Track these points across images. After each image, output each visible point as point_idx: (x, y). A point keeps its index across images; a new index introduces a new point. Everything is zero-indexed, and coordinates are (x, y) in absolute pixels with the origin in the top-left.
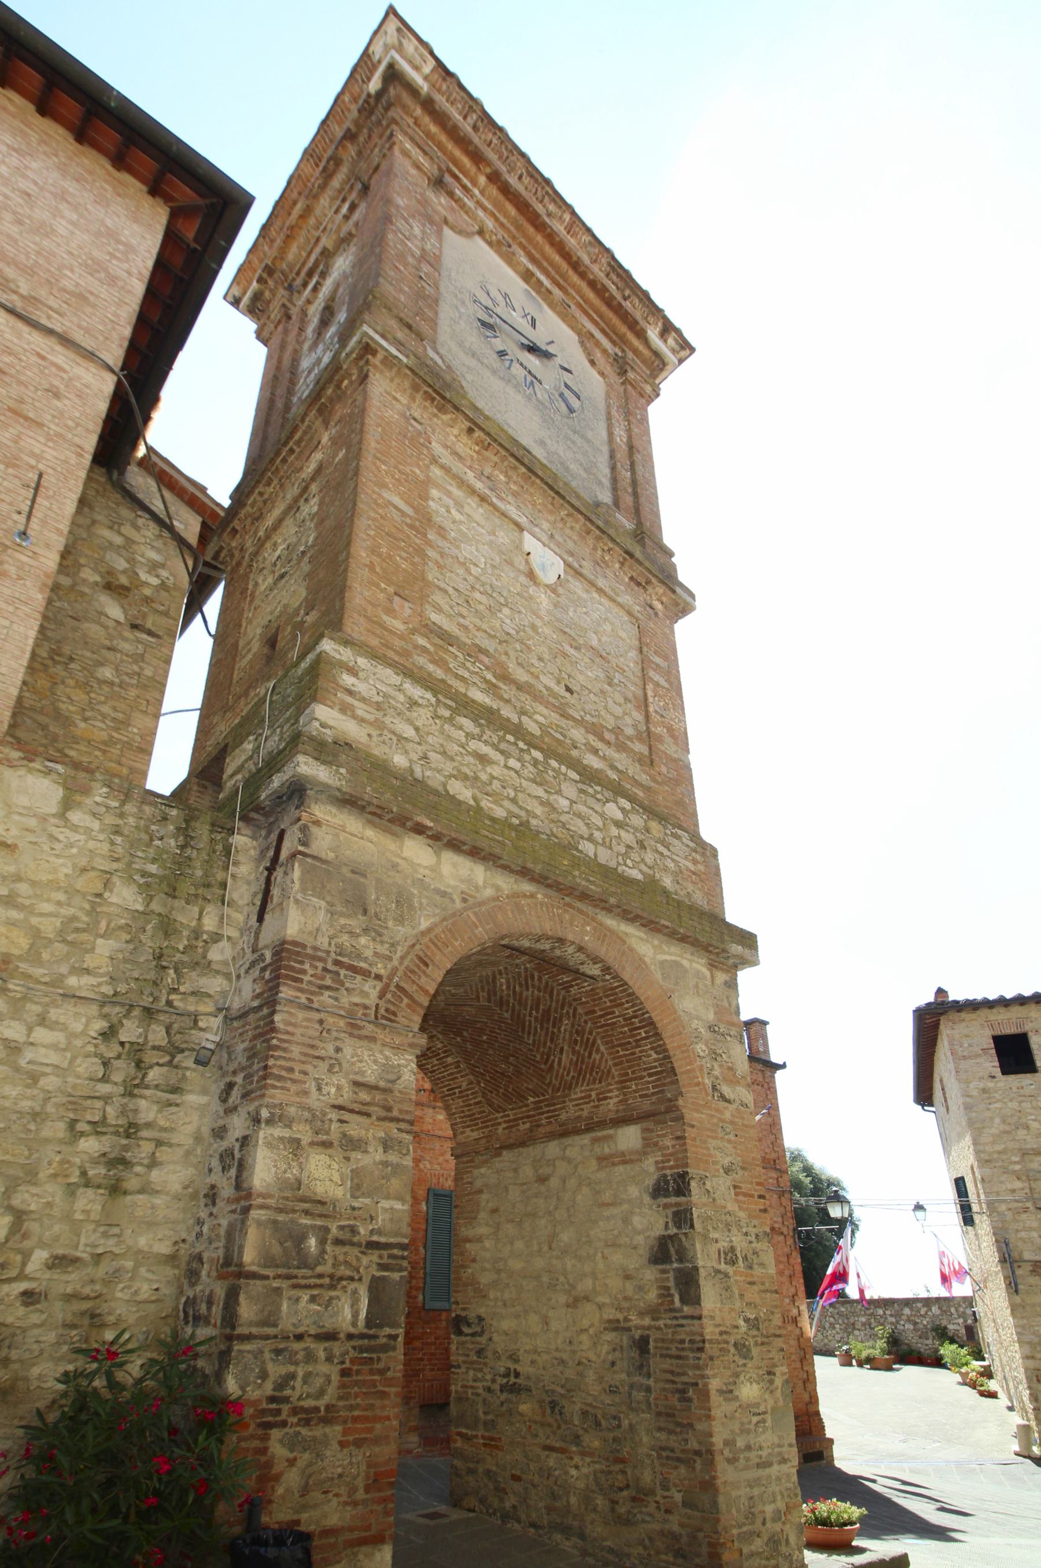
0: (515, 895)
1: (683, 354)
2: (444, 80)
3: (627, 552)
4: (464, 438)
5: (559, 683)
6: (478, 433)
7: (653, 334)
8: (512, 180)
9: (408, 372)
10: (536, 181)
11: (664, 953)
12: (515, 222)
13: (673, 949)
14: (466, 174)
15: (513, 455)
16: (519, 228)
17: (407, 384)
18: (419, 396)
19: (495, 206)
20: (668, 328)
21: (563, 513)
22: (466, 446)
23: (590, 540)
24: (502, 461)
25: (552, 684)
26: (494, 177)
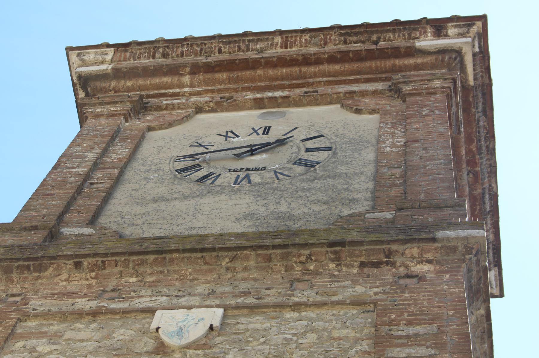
2: (126, 51)
3: (332, 244)
6: (86, 263)
8: (215, 57)
10: (235, 42)
12: (230, 80)
15: (132, 254)
16: (237, 80)
18: (15, 276)
19: (207, 85)
20: (439, 26)
22: (79, 281)
23: (278, 265)
24: (127, 266)
26: (195, 69)
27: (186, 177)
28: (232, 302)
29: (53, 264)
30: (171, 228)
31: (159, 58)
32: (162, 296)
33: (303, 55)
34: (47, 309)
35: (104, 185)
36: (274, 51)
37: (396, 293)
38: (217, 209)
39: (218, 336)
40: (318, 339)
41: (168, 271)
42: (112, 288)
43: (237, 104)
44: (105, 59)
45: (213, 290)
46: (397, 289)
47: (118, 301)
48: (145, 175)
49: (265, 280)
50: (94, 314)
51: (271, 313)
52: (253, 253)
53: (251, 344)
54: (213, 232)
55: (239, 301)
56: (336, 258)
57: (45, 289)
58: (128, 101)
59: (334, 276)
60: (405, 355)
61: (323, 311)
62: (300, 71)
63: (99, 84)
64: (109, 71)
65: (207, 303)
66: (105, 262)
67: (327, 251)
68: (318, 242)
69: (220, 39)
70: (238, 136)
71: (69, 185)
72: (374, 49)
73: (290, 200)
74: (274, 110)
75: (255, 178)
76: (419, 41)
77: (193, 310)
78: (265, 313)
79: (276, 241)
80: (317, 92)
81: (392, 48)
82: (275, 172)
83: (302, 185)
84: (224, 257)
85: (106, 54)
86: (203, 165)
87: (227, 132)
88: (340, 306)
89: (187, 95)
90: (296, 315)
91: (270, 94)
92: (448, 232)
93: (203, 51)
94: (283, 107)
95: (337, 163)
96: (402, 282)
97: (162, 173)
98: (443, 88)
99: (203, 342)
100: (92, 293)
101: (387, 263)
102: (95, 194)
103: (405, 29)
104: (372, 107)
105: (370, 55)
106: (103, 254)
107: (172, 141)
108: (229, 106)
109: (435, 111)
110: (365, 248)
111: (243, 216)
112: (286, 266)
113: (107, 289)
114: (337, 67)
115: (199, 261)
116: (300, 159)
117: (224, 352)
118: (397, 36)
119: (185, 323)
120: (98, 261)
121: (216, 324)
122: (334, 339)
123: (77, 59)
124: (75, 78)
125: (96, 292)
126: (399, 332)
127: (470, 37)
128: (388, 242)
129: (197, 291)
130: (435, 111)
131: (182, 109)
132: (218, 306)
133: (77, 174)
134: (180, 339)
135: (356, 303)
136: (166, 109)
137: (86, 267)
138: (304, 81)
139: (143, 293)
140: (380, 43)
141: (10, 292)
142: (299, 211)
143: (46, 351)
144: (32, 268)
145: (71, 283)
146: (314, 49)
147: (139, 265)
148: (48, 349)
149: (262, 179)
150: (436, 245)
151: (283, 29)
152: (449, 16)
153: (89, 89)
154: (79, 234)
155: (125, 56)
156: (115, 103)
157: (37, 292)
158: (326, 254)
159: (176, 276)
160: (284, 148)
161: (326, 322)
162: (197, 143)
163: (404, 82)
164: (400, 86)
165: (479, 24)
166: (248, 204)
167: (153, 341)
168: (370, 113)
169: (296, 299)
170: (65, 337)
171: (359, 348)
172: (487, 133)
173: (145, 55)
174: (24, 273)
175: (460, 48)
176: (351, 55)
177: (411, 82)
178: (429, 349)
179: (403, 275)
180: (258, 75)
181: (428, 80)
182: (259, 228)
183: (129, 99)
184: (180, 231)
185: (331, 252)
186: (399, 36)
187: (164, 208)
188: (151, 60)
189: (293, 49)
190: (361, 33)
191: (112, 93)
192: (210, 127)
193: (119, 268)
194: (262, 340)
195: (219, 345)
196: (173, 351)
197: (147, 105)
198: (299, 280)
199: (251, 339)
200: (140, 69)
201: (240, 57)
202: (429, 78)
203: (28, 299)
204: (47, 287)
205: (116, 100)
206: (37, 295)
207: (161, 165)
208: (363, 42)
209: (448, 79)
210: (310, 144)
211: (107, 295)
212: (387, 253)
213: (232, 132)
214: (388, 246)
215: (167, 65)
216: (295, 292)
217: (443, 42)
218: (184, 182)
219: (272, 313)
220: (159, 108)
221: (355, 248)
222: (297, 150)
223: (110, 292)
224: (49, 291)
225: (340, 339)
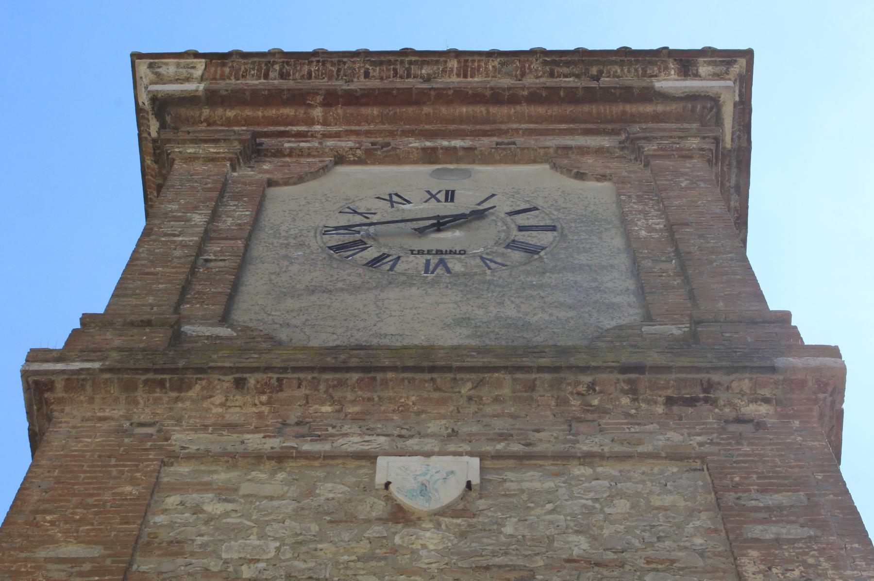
2: (224, 65)
3: (625, 369)
6: (252, 380)
8: (359, 84)
9: (107, 376)
10: (389, 62)
14: (294, 122)
15: (324, 369)
16: (393, 120)
17: (115, 391)
18: (141, 395)
19: (348, 123)
20: (686, 61)
21: (466, 389)
22: (242, 407)
26: (331, 99)
28: (489, 448)
29: (201, 379)
30: (349, 333)
31: (275, 79)
32: (378, 435)
33: (492, 89)
34: (202, 447)
35: (227, 264)
36: (448, 80)
38: (411, 309)
39: (481, 498)
40: (632, 507)
41: (380, 398)
42: (296, 420)
43: (396, 155)
44: (191, 74)
45: (453, 430)
46: (729, 438)
47: (311, 440)
48: (283, 252)
49: (528, 418)
50: (280, 458)
51: (548, 464)
53: (533, 512)
54: (417, 342)
55: (500, 446)
56: (631, 389)
57: (190, 417)
58: (236, 140)
59: (632, 416)
60: (772, 536)
61: (627, 466)
62: (488, 112)
63: (184, 112)
64: (201, 94)
65: (451, 447)
66: (282, 380)
67: (618, 379)
68: (605, 365)
70: (409, 202)
71: (175, 260)
72: (595, 88)
74: (451, 167)
75: (455, 265)
76: (659, 81)
78: (540, 466)
80: (514, 143)
81: (621, 88)
82: (482, 258)
83: (528, 279)
85: (193, 68)
86: (370, 242)
87: (390, 195)
88: (652, 461)
89: (319, 136)
90: (588, 471)
91: (445, 143)
92: (791, 359)
93: (342, 72)
94: (464, 163)
95: (571, 250)
96: (732, 428)
97: (308, 251)
98: (702, 149)
99: (461, 506)
100: (267, 426)
101: (706, 400)
102: (218, 277)
103: (637, 61)
104: (600, 170)
105: (590, 96)
107: (309, 203)
108: (386, 156)
109: (699, 183)
110: (673, 376)
111: (454, 320)
112: (557, 399)
113: (288, 422)
114: (541, 110)
115: (427, 385)
116: (514, 241)
118: (626, 71)
119: (428, 477)
120: (271, 378)
121: (476, 481)
122: (657, 508)
123: (148, 71)
124: (144, 98)
126: (753, 502)
127: (730, 79)
128: (708, 370)
129: (429, 431)
130: (699, 183)
131: (314, 156)
132: (471, 454)
133: (183, 245)
135: (675, 456)
136: (290, 155)
137: (252, 387)
138: (493, 127)
139: (346, 429)
140: (602, 79)
141: (135, 419)
142: (536, 318)
143: (219, 512)
144: (168, 385)
146: (505, 82)
147: (334, 387)
148: (222, 509)
149: (465, 266)
150: (776, 377)
152: (700, 48)
153: (168, 119)
154: (211, 336)
156: (216, 141)
157: (179, 420)
158: (616, 383)
159: (392, 407)
160: (483, 223)
161: (637, 483)
162: (349, 208)
163: (645, 138)
164: (641, 143)
165: (742, 62)
166: (455, 303)
167: (383, 503)
168: (598, 180)
169: (585, 448)
170: (241, 493)
171: (698, 523)
172: (738, 218)
173: (252, 72)
174: (155, 392)
175: (717, 94)
176: (562, 93)
177: (656, 138)
178: (806, 529)
179: (731, 419)
180: (426, 114)
181: (680, 138)
182: (484, 339)
184: (364, 339)
185: (624, 381)
186: (629, 71)
187: (328, 302)
188: (263, 81)
190: (575, 63)
192: (360, 185)
193: (303, 391)
194: (549, 507)
195: (485, 512)
197: (260, 148)
198: (579, 420)
199: (532, 505)
200: (248, 93)
201: (399, 86)
202: (681, 134)
204: (194, 414)
205: (216, 137)
206: (181, 426)
207: (302, 238)
208: (577, 76)
209: (708, 137)
210: (521, 220)
212: (705, 385)
214: (707, 376)
215: (288, 90)
216: (580, 438)
218: (348, 266)
219: (552, 467)
220: (279, 153)
221: (660, 376)
222: (505, 228)
223: (294, 425)
224: (198, 421)
225: (665, 509)
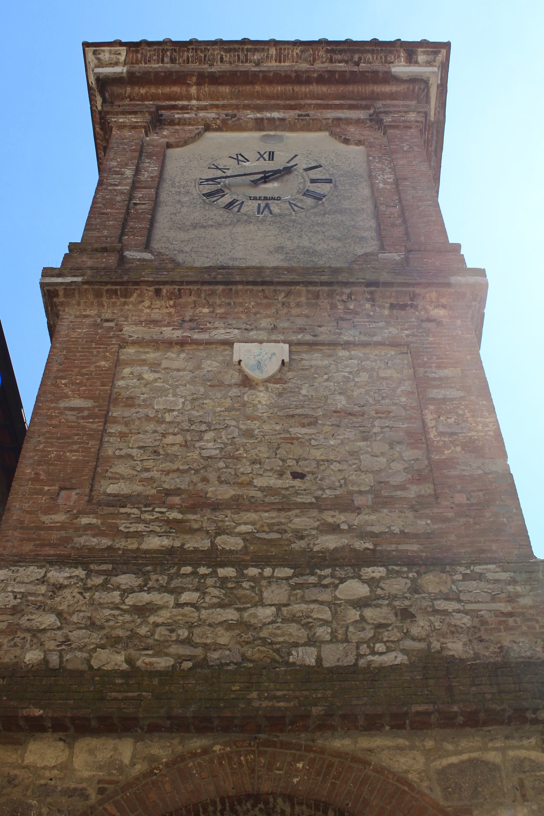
0: (179, 760)
1: (440, 58)
2: (137, 52)
4: (158, 303)
5: (281, 474)
6: (165, 290)
7: (400, 68)
8: (217, 68)
9: (86, 287)
10: (235, 50)
11: (448, 754)
13: (464, 743)
15: (203, 283)
17: (91, 297)
18: (104, 299)
19: (212, 99)
20: (410, 50)
22: (160, 309)
23: (324, 303)
25: (273, 481)
26: (204, 79)
27: (214, 202)
29: (136, 289)
31: (167, 63)
33: (296, 71)
36: (270, 64)
37: (423, 336)
40: (369, 378)
41: (234, 303)
44: (118, 59)
47: (198, 332)
48: (177, 198)
50: (182, 343)
52: (304, 289)
53: (317, 381)
54: (254, 264)
55: (300, 337)
56: (371, 298)
57: (132, 315)
61: (367, 350)
63: (118, 90)
64: (125, 75)
65: (273, 337)
69: (221, 45)
70: (248, 161)
73: (310, 234)
74: (272, 133)
76: (394, 67)
77: (264, 344)
78: (321, 350)
79: (323, 277)
80: (308, 115)
82: (290, 203)
84: (280, 291)
85: (119, 54)
86: (227, 191)
89: (195, 109)
92: (459, 278)
93: (207, 58)
96: (424, 325)
97: (191, 197)
98: (417, 122)
99: (279, 377)
100: (174, 322)
101: (412, 306)
104: (358, 137)
106: (179, 282)
109: (414, 147)
110: (395, 289)
112: (331, 304)
116: (308, 190)
117: (297, 387)
119: (261, 357)
120: (175, 289)
124: (92, 79)
125: (177, 322)
127: (436, 66)
130: (414, 147)
131: (192, 125)
132: (284, 342)
134: (262, 372)
135: (394, 344)
136: (178, 124)
139: (217, 324)
141: (104, 316)
145: (154, 311)
146: (304, 66)
147: (209, 295)
151: (277, 39)
153: (107, 95)
155: (137, 57)
156: (135, 113)
157: (126, 318)
159: (241, 309)
166: (275, 236)
168: (357, 144)
170: (162, 366)
171: (403, 388)
174: (112, 298)
177: (391, 112)
181: (405, 112)
183: (147, 109)
186: (377, 59)
189: (286, 64)
190: (345, 51)
191: (127, 102)
194: (326, 377)
196: (257, 384)
198: (343, 319)
199: (316, 376)
200: (152, 75)
202: (405, 109)
203: (121, 325)
207: (188, 188)
208: (346, 62)
211: (186, 325)
213: (241, 155)
215: (176, 72)
216: (342, 331)
217: (414, 70)
218: (214, 208)
220: (172, 123)
